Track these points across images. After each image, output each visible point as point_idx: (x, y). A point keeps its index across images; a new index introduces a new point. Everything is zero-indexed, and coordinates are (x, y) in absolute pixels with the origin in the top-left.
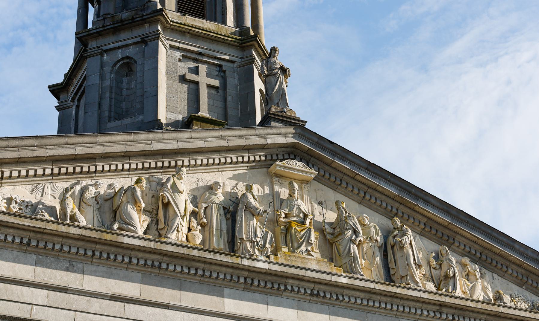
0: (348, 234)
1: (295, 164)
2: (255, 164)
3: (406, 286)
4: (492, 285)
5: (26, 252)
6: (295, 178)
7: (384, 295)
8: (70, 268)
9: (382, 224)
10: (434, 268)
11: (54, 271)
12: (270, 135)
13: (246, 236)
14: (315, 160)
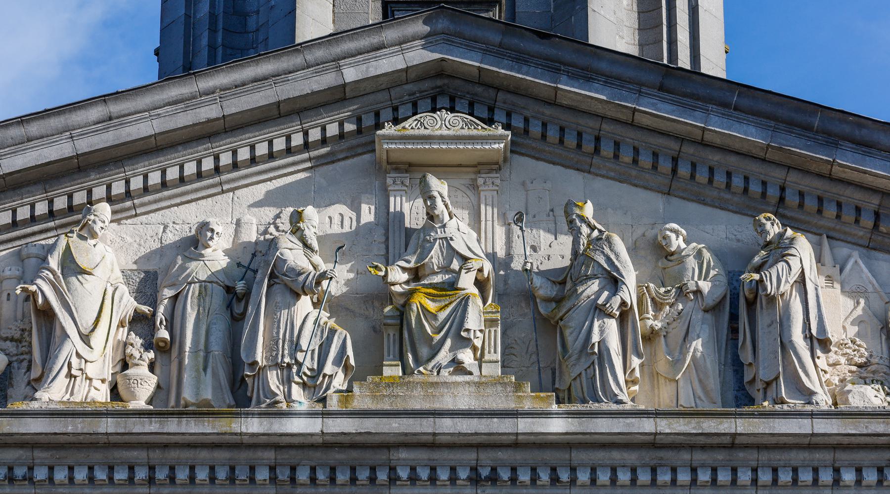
1: (439, 123)
2: (328, 149)
3: (778, 407)
6: (455, 163)
7: (703, 447)
9: (738, 241)
12: (353, 56)
13: (269, 354)
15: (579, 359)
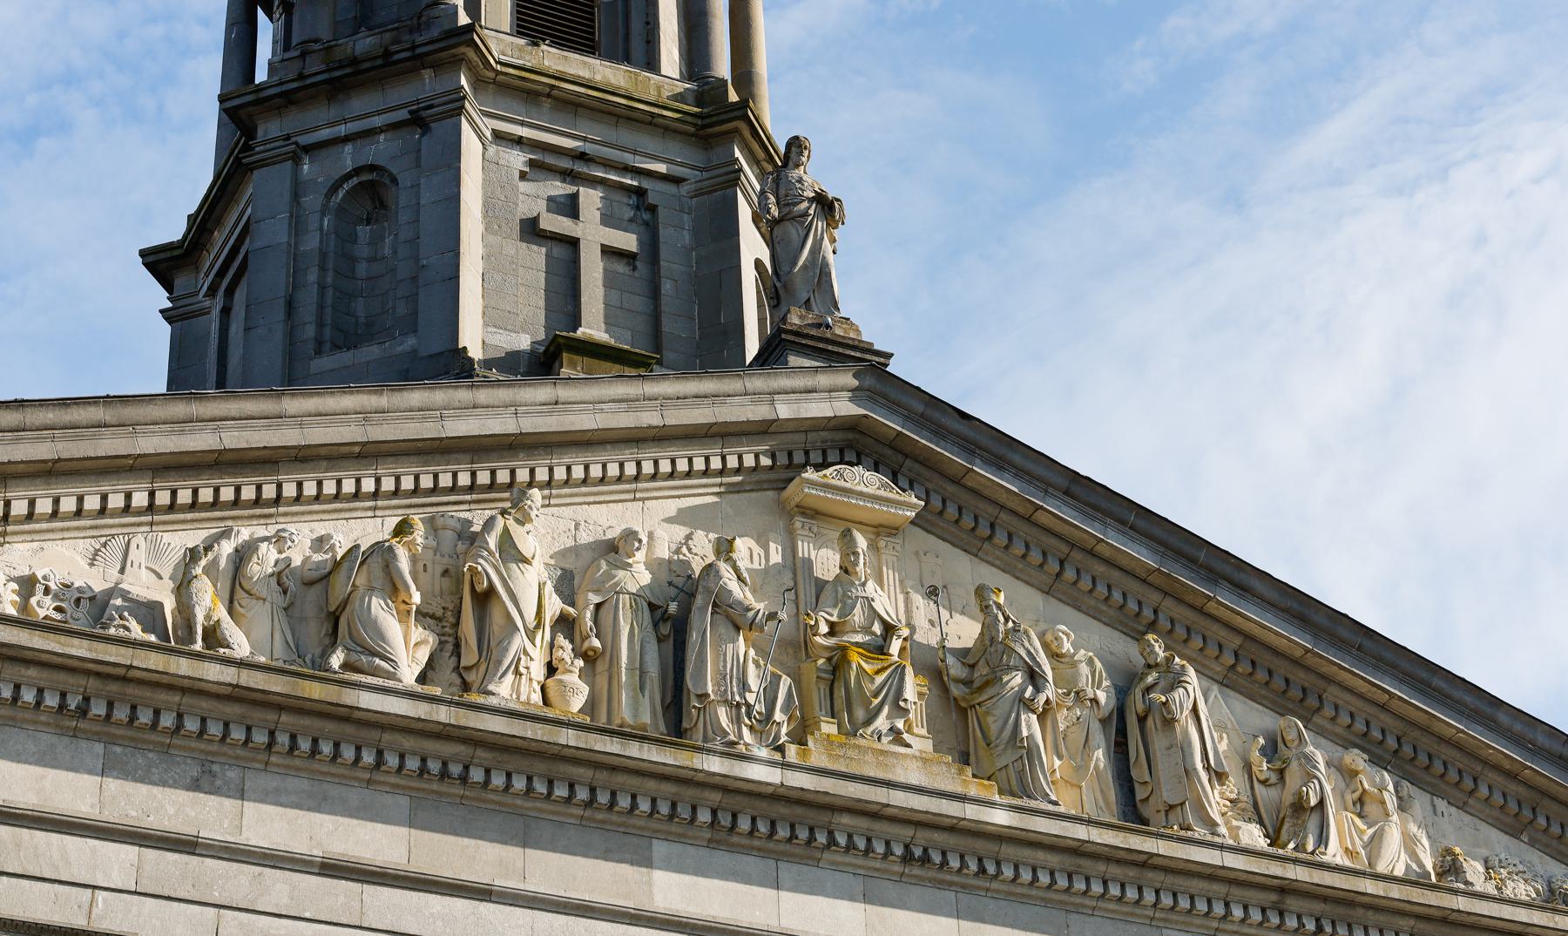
0: (1013, 683)
1: (858, 478)
2: (740, 478)
3: (1183, 833)
4: (1431, 830)
5: (75, 734)
6: (858, 519)
7: (1119, 862)
8: (205, 782)
9: (1111, 653)
10: (1264, 782)
11: (156, 790)
12: (787, 393)
13: (716, 688)
14: (917, 466)
15: (1005, 750)
